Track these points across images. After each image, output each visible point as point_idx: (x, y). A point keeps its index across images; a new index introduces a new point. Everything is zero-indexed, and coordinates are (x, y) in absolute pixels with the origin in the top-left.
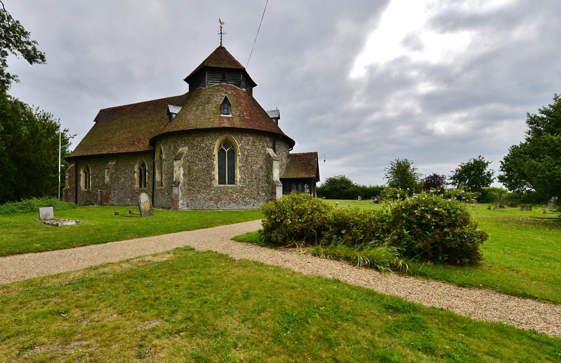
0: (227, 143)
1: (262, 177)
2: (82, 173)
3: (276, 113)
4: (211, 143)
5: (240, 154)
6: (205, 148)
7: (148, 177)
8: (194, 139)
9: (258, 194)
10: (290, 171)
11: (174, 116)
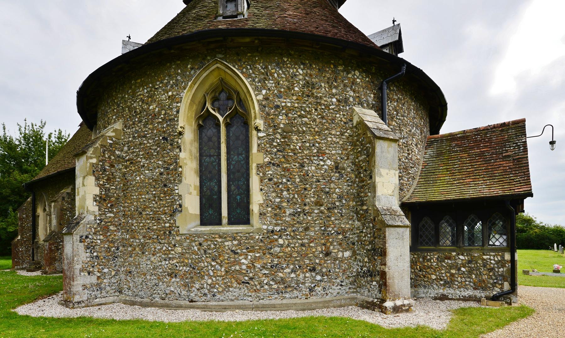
1: (340, 198)
2: (40, 211)
3: (392, 32)
4: (171, 98)
5: (260, 122)
8: (134, 94)
9: (328, 254)
10: (435, 181)
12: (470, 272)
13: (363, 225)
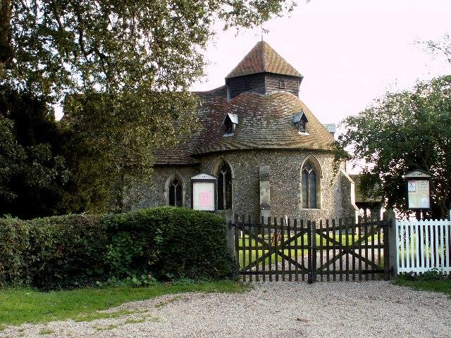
0: (309, 164)
6: (290, 168)
11: (235, 126)
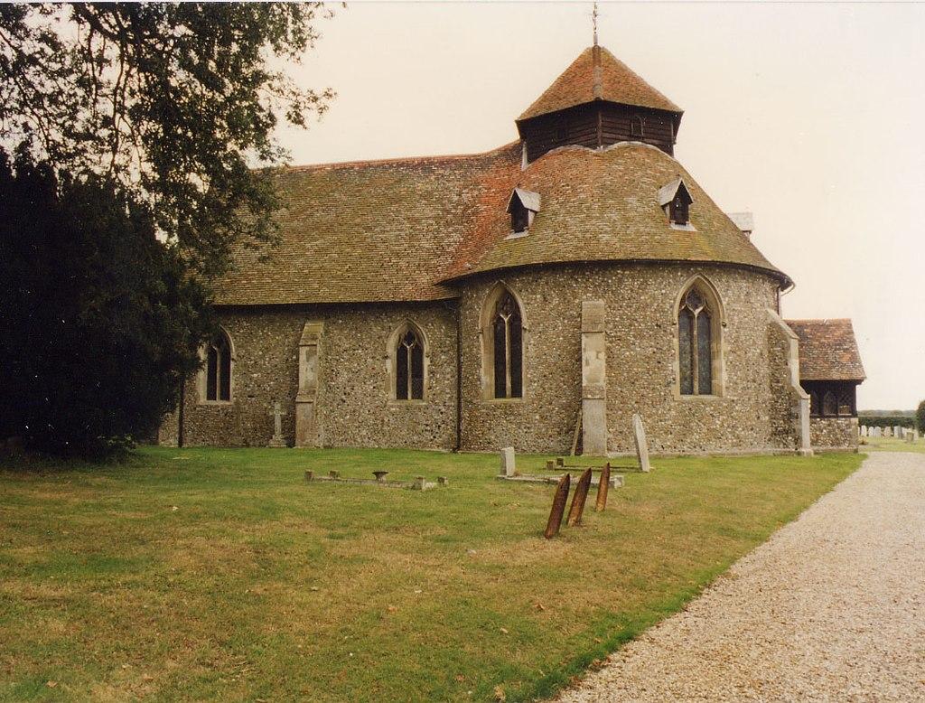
0: (694, 296)
7: (432, 372)
11: (531, 216)
12: (829, 432)
13: (779, 398)
